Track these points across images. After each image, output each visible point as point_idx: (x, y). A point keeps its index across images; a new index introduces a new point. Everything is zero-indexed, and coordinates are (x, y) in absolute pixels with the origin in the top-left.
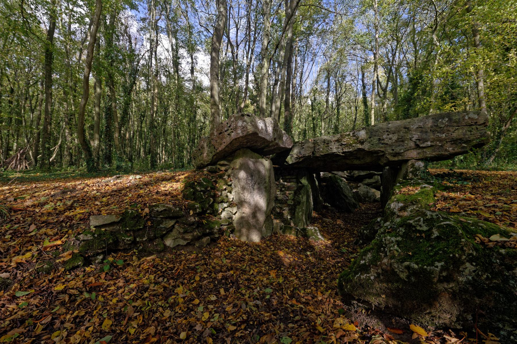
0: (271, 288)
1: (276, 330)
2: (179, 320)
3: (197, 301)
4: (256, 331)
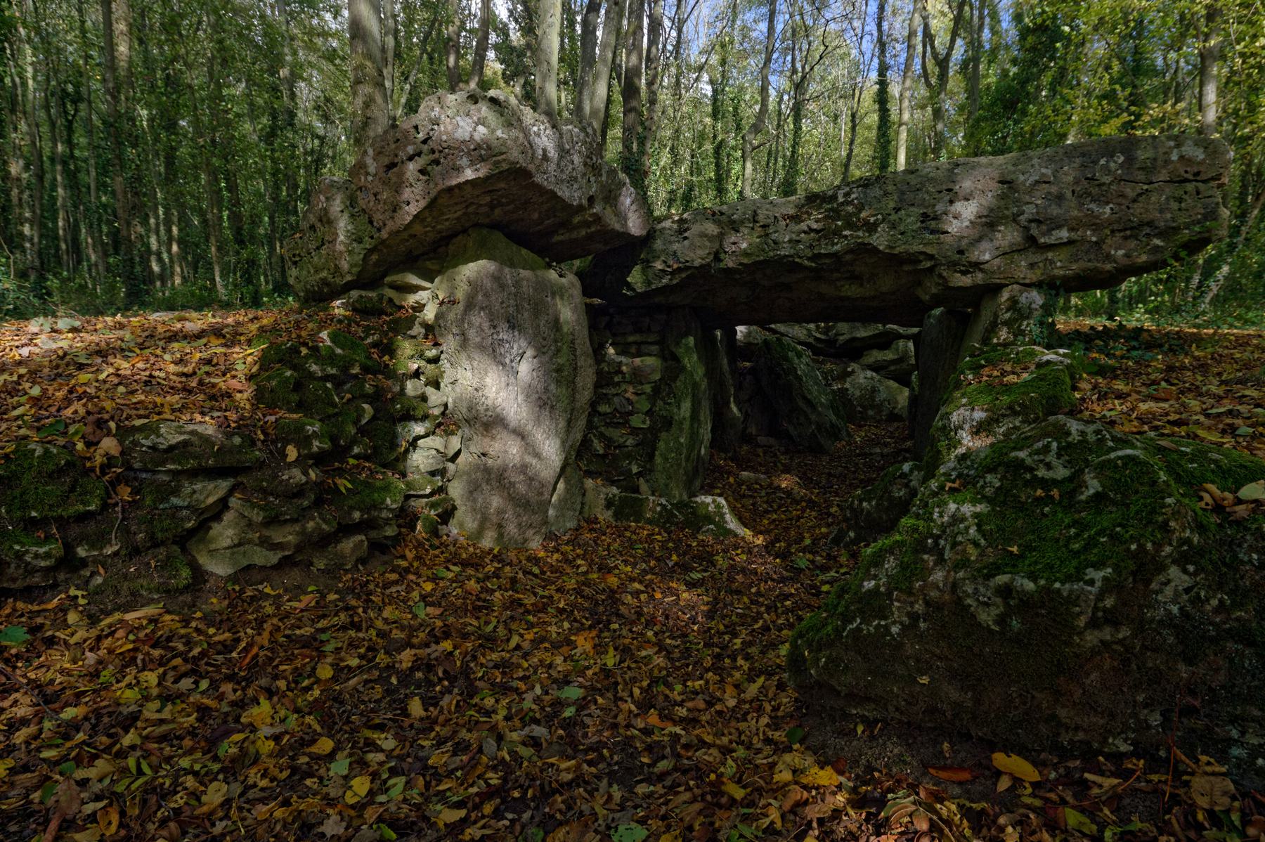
0: (581, 686)
1: (598, 809)
2: (261, 810)
3: (326, 745)
4: (532, 817)
